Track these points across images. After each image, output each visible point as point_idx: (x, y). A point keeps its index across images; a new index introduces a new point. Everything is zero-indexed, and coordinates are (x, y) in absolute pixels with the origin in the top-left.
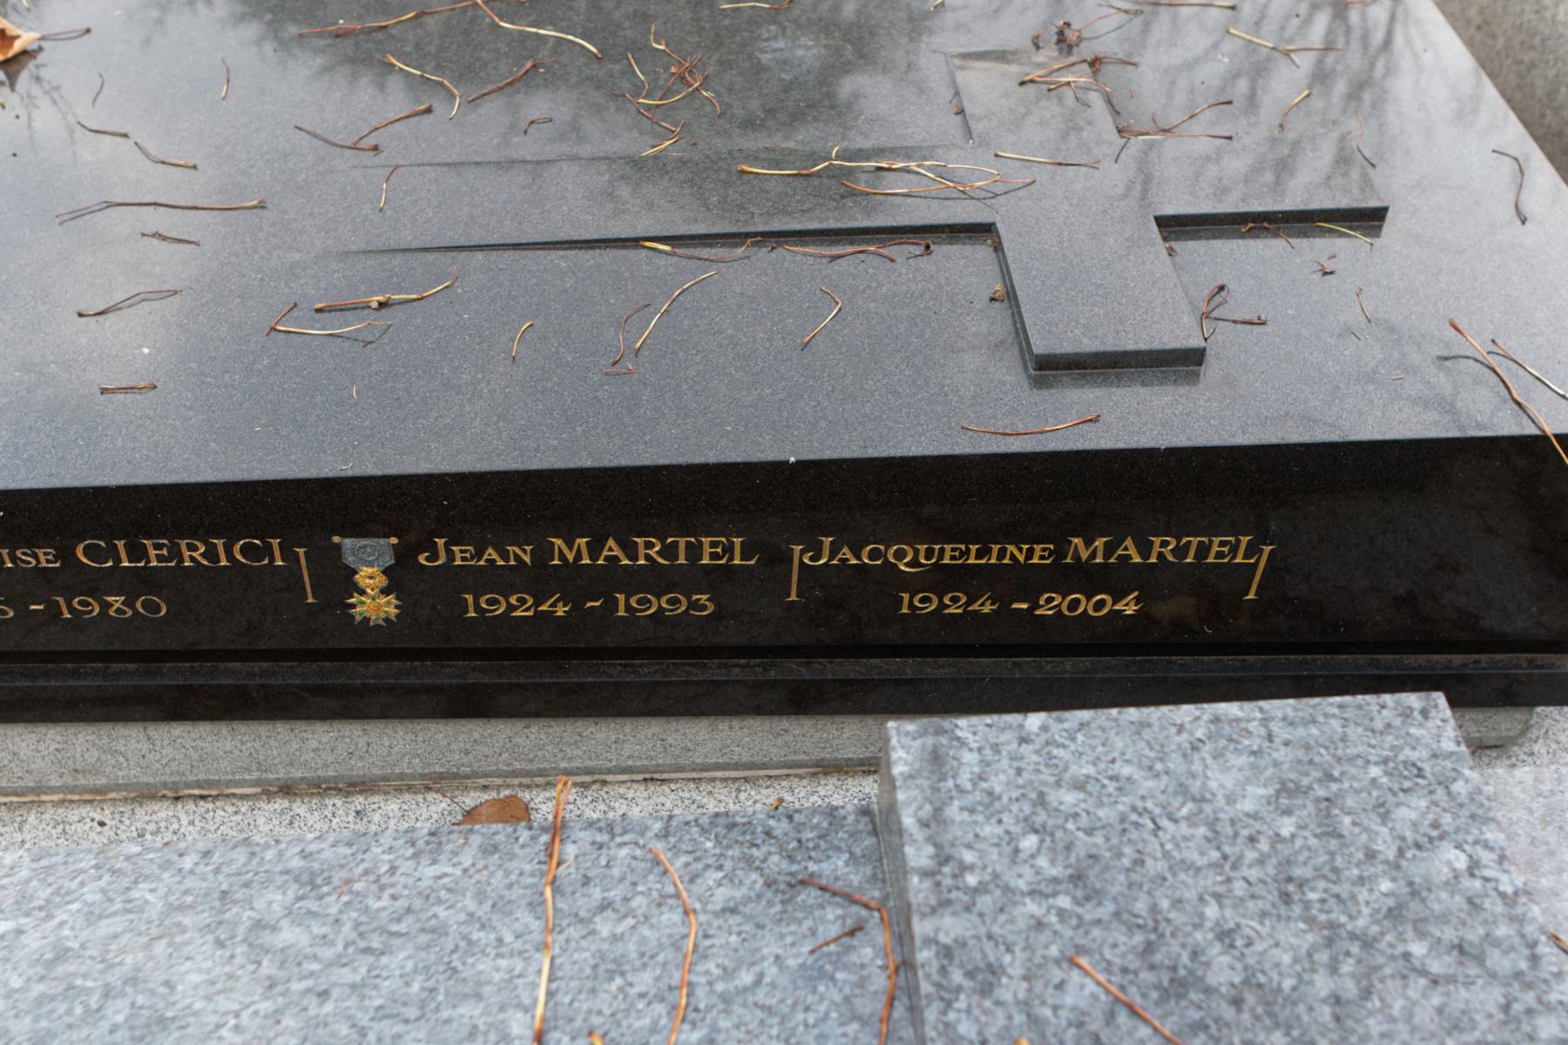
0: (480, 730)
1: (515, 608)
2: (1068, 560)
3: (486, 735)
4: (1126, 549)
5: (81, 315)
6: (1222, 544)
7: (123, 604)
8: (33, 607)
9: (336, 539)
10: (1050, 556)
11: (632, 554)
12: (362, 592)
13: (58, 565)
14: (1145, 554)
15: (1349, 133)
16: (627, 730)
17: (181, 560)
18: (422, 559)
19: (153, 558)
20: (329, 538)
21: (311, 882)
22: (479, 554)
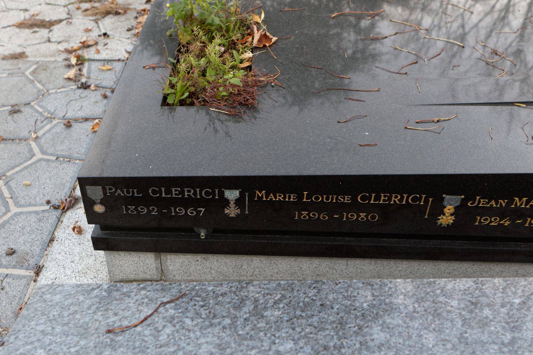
0: (457, 266)
3: (459, 267)
4: (271, 197)
5: (339, 122)
6: (483, 201)
7: (364, 216)
8: (164, 211)
9: (223, 190)
11: (276, 198)
12: (444, 215)
13: (180, 196)
14: (497, 204)
16: (507, 268)
20: (442, 195)
22: (488, 203)
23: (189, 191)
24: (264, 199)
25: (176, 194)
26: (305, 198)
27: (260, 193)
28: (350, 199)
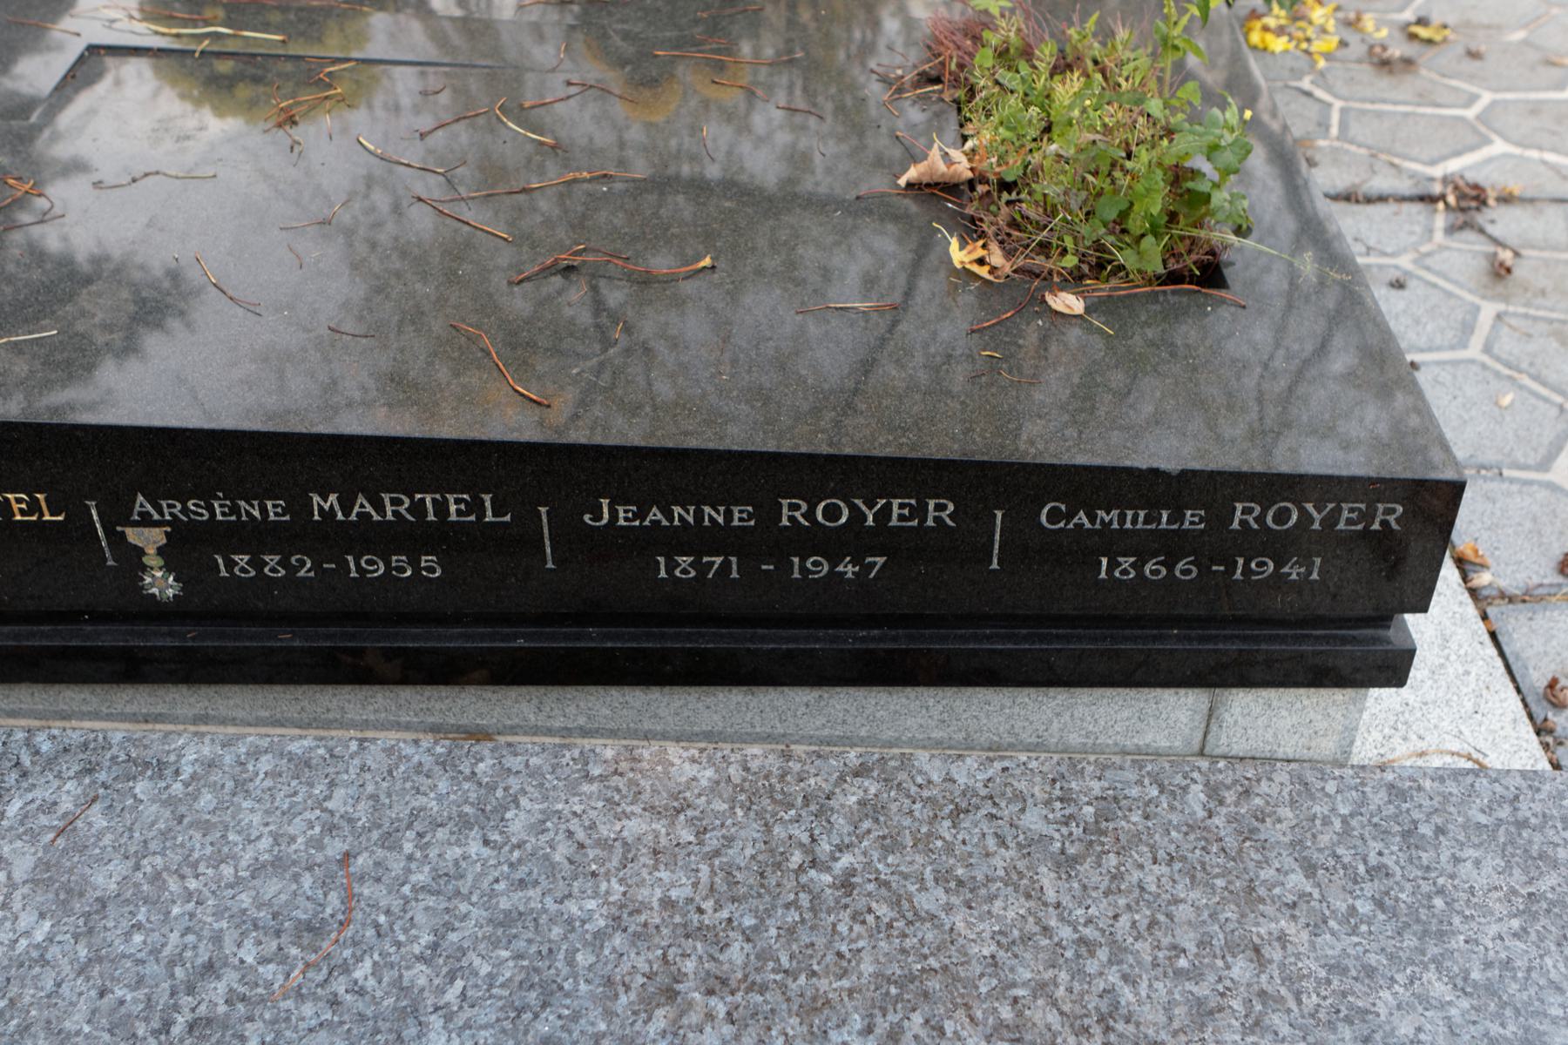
7: (690, 565)
10: (1200, 523)
14: (1092, 521)
15: (266, 131)
17: (239, 516)
18: (587, 518)
19: (16, 511)
23: (396, 502)
26: (489, 512)
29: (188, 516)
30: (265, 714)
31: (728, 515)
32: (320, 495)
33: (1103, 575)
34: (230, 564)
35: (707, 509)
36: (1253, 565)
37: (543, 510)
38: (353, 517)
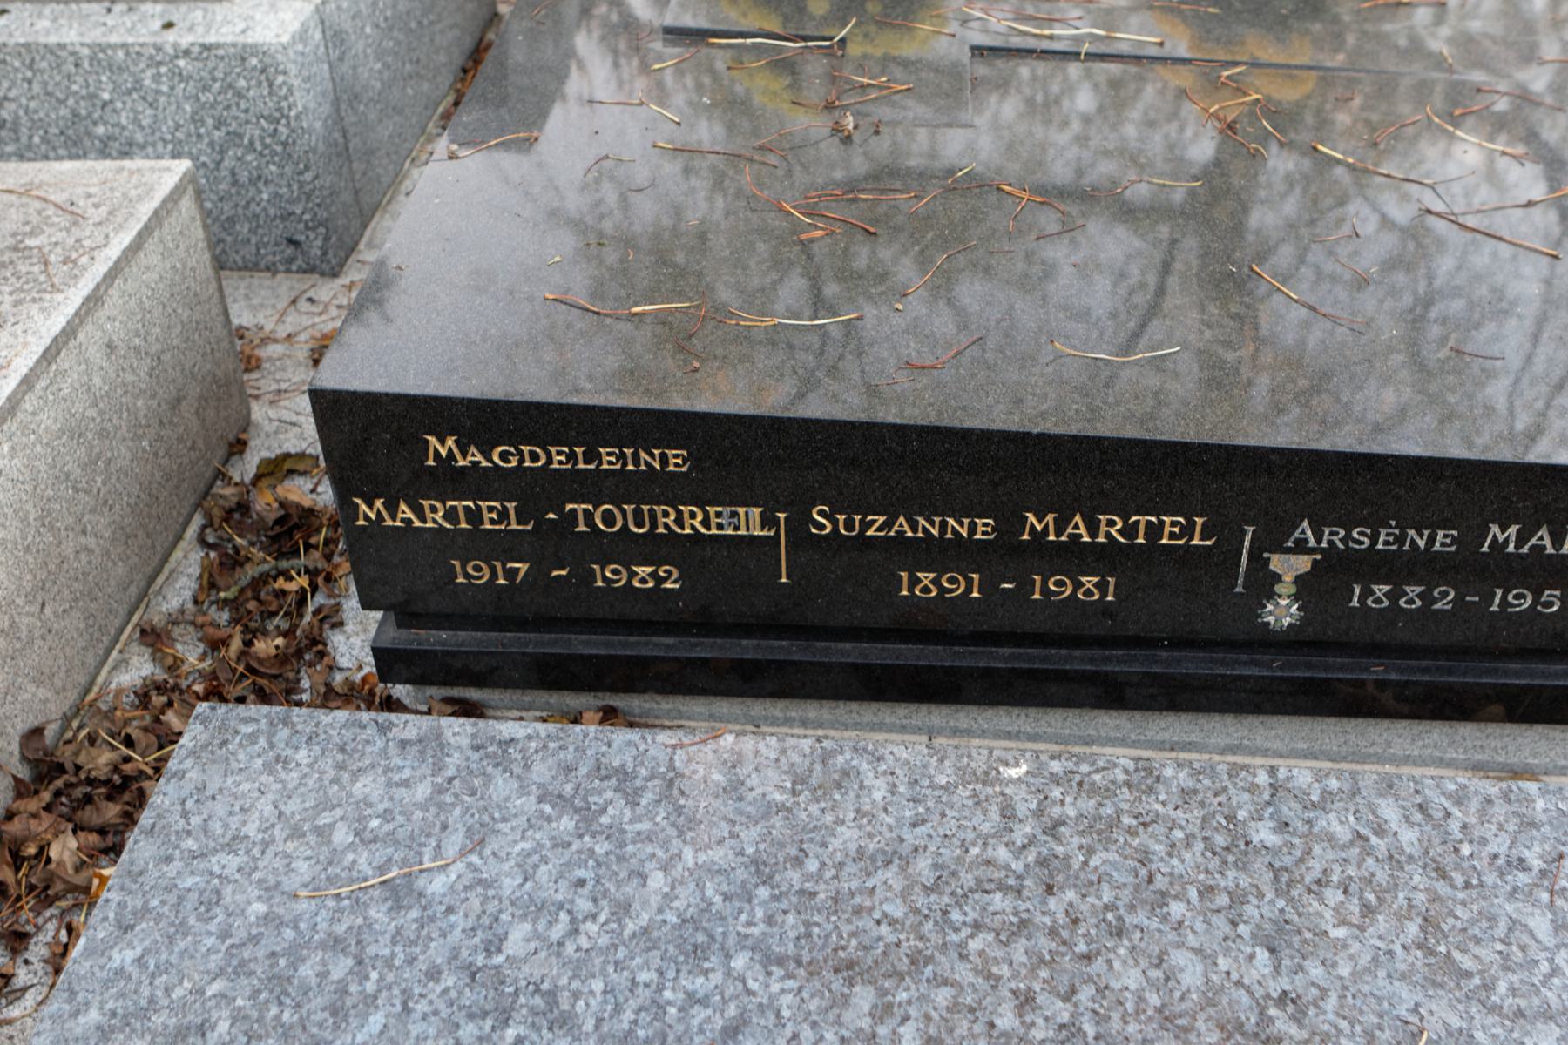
1: (665, 580)
2: (1026, 537)
14: (1093, 531)
19: (486, 520)
21: (1050, 890)
24: (1052, 538)
25: (984, 533)
27: (1040, 522)
28: (994, 530)
29: (1346, 545)
30: (1302, 745)
31: (973, 529)
32: (1036, 515)
33: (1355, 603)
34: (914, 581)
35: (951, 521)
36: (1510, 598)
37: (782, 516)
38: (1525, 550)
